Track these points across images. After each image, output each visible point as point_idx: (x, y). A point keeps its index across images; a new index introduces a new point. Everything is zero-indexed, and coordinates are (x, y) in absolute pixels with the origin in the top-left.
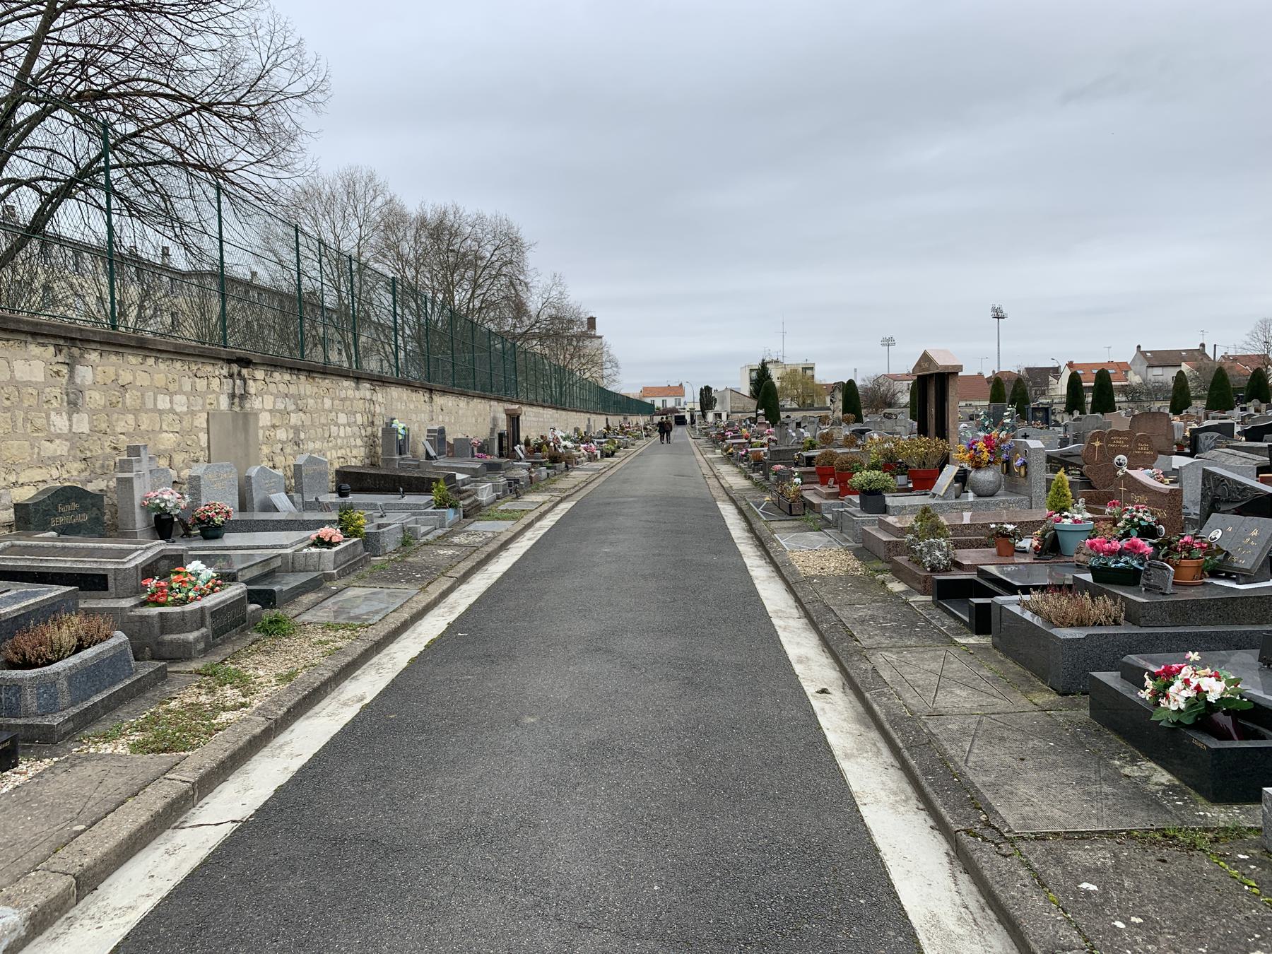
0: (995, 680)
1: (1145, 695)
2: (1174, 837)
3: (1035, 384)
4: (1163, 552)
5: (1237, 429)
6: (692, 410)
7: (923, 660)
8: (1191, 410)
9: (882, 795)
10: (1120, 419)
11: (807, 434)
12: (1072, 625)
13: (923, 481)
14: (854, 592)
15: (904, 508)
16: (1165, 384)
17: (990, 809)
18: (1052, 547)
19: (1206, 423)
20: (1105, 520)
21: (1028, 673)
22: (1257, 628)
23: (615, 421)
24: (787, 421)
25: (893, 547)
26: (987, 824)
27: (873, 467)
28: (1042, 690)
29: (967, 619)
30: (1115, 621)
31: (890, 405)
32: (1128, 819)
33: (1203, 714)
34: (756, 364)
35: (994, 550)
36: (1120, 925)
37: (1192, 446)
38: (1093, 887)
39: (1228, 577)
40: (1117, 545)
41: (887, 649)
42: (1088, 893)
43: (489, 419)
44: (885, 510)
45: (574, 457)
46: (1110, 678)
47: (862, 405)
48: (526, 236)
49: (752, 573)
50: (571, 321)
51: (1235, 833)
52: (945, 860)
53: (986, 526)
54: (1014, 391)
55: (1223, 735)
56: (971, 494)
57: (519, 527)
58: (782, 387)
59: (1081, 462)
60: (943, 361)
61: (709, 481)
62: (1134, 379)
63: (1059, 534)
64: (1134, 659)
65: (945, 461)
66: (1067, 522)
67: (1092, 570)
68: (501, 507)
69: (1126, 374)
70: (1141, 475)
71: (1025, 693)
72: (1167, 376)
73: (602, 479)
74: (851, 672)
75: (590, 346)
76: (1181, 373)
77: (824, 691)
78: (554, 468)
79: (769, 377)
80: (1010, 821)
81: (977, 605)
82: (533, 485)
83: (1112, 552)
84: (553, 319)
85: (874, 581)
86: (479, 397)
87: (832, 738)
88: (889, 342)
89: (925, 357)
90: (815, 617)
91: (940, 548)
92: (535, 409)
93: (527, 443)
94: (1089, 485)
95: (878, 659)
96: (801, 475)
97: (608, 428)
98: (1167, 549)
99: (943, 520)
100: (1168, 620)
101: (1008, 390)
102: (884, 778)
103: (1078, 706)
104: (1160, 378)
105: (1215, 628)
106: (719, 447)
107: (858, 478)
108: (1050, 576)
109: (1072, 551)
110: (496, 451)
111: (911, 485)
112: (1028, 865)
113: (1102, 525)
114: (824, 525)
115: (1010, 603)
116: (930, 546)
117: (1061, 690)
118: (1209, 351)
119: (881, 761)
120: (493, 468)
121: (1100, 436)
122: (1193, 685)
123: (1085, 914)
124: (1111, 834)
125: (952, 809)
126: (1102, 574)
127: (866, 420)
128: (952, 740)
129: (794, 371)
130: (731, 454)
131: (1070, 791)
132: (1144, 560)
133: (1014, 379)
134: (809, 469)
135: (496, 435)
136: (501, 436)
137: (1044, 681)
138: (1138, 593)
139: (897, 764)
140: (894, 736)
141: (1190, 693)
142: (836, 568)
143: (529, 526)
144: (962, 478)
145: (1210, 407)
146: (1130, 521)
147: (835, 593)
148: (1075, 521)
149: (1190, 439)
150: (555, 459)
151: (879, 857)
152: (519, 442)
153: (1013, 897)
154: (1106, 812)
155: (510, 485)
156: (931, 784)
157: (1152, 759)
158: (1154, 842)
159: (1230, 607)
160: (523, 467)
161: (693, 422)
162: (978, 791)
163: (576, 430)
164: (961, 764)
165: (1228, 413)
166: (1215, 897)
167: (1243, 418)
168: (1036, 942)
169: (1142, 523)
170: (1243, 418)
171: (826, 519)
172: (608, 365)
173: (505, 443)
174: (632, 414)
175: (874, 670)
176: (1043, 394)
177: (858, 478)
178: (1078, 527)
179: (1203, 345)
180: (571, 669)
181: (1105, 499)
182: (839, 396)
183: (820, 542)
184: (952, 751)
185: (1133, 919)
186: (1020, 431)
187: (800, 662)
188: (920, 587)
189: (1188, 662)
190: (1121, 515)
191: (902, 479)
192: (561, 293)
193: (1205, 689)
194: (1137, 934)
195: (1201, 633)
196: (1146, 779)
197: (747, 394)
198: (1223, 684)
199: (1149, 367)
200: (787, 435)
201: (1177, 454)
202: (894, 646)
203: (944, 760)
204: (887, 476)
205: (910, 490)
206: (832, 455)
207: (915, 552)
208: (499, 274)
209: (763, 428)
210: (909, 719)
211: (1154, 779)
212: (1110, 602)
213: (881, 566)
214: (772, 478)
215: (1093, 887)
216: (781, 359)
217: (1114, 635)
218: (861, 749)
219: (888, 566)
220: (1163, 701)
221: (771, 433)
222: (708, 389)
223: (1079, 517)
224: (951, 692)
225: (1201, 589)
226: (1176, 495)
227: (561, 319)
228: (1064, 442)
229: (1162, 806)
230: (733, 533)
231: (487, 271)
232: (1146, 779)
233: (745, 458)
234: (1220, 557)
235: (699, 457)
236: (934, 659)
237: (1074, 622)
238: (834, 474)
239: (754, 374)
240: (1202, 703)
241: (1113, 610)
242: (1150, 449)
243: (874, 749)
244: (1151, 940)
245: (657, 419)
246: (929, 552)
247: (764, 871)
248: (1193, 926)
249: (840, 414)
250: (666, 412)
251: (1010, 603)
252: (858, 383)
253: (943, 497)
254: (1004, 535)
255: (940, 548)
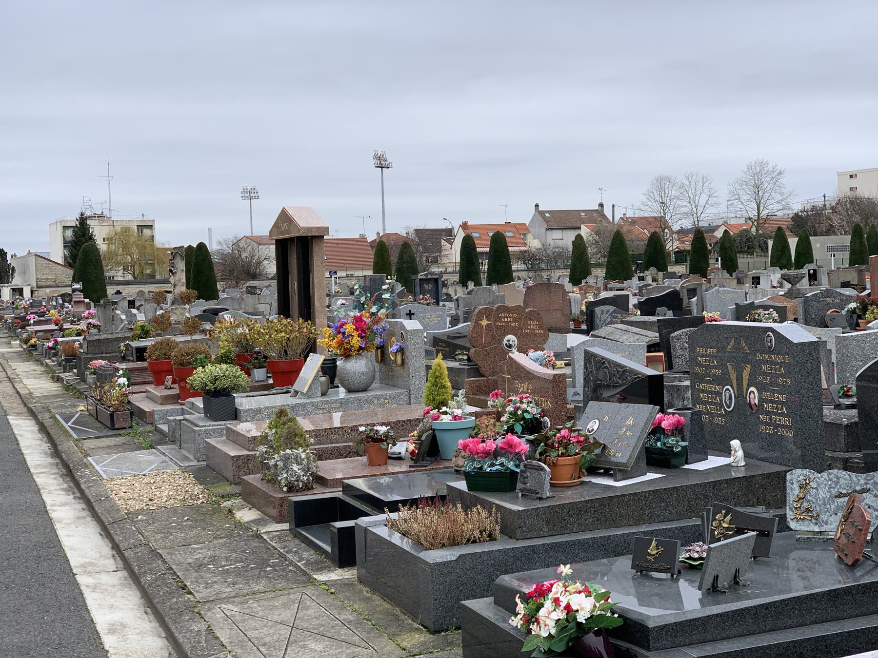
1: (516, 622)
3: (426, 250)
4: (539, 450)
5: (633, 301)
7: (273, 608)
8: (590, 280)
10: (513, 293)
12: (444, 546)
13: (284, 375)
14: (192, 527)
15: (257, 408)
16: (564, 249)
18: (430, 450)
19: (604, 295)
20: (489, 414)
21: (397, 611)
24: (116, 298)
25: (244, 464)
27: (224, 359)
28: (412, 630)
29: (328, 548)
30: (490, 536)
31: (254, 276)
34: (72, 220)
35: (365, 459)
37: (588, 323)
39: (607, 473)
41: (228, 600)
44: (235, 415)
46: (481, 606)
47: (219, 275)
49: (53, 515)
53: (355, 429)
54: (401, 257)
56: (342, 390)
58: (109, 252)
59: (468, 345)
60: (305, 222)
62: (534, 244)
63: (437, 434)
64: (508, 580)
65: (312, 348)
66: (446, 419)
69: (525, 239)
70: (528, 361)
71: (392, 637)
72: (565, 240)
74: (180, 637)
76: (579, 237)
79: (91, 238)
81: (340, 529)
83: (487, 454)
85: (218, 510)
88: (250, 195)
89: (284, 217)
94: (476, 371)
96: (128, 374)
99: (305, 424)
100: (545, 529)
101: (394, 258)
103: (451, 644)
104: (560, 243)
106: (17, 337)
107: (200, 376)
108: (429, 486)
109: (451, 454)
111: (271, 381)
114: (159, 439)
115: (375, 524)
116: (286, 459)
117: (432, 626)
118: (608, 212)
121: (487, 313)
122: (563, 604)
127: (222, 295)
129: (126, 231)
130: (34, 346)
132: (520, 460)
133: (401, 243)
134: (140, 364)
137: (414, 616)
138: (514, 501)
141: (561, 614)
142: (169, 498)
144: (329, 369)
145: (609, 276)
146: (514, 414)
147: (166, 531)
148: (455, 418)
149: (587, 314)
165: (626, 283)
167: (641, 289)
169: (527, 416)
170: (641, 289)
171: (161, 432)
175: (210, 630)
176: (435, 261)
177: (200, 376)
178: (459, 424)
179: (601, 205)
181: (488, 389)
182: (181, 265)
183: (150, 463)
186: (403, 308)
187: (112, 631)
188: (274, 512)
189: (559, 577)
190: (504, 407)
191: (259, 374)
193: (574, 608)
195: (557, 544)
198: (591, 600)
199: (548, 229)
200: (113, 319)
204: (236, 370)
205: (268, 387)
206: (170, 345)
207: (269, 468)
209: (81, 308)
212: (484, 513)
213: (229, 489)
214: (90, 378)
216: (106, 213)
217: (489, 553)
220: (534, 627)
221: (92, 314)
223: (458, 412)
224: (304, 647)
225: (580, 490)
226: (559, 381)
228: (455, 321)
233: (52, 352)
234: (598, 451)
236: (286, 606)
237: (445, 541)
238: (167, 368)
239: (69, 234)
241: (487, 524)
242: (541, 328)
246: (286, 468)
249: (184, 289)
251: (376, 524)
252: (213, 247)
253: (307, 395)
254: (375, 440)
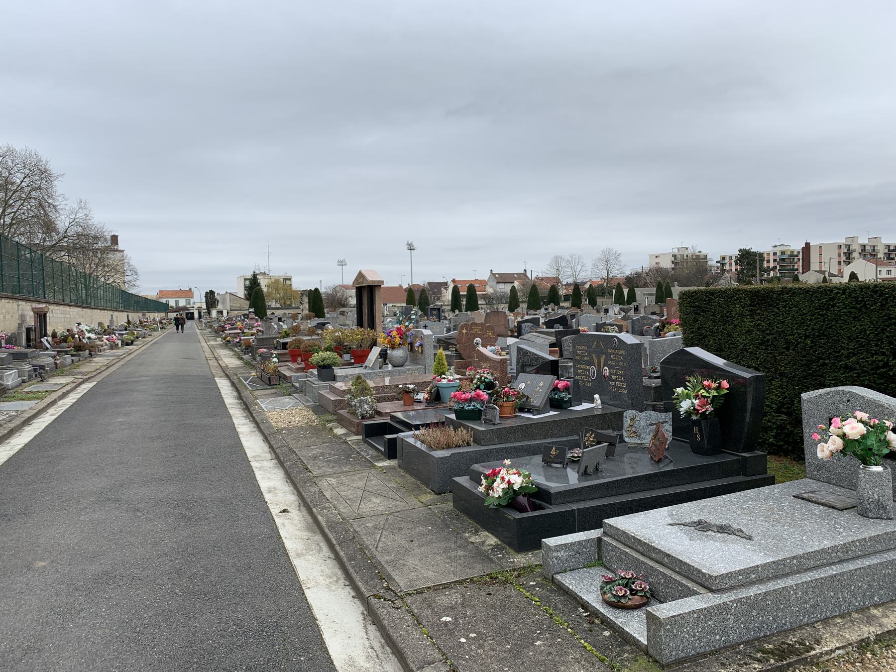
0: (398, 489)
1: (482, 489)
2: (497, 578)
5: (542, 321)
6: (199, 309)
8: (519, 310)
9: (321, 580)
11: (285, 327)
13: (360, 358)
14: (311, 437)
15: (346, 375)
17: (390, 578)
18: (436, 398)
19: (526, 317)
21: (419, 482)
22: (543, 441)
23: (135, 317)
25: (339, 404)
26: (388, 589)
27: (327, 349)
29: (383, 449)
31: (344, 306)
32: (471, 571)
33: (512, 498)
34: (249, 275)
35: (402, 402)
36: (463, 640)
37: (518, 332)
38: (449, 619)
39: (529, 411)
40: (468, 395)
41: (330, 476)
42: (446, 623)
43: (16, 316)
44: (334, 378)
45: (98, 346)
47: (325, 305)
48: (54, 167)
49: (238, 430)
50: (96, 238)
51: (529, 569)
52: (361, 617)
53: (397, 386)
55: (522, 510)
56: (390, 365)
57: (42, 405)
58: (268, 292)
60: (371, 278)
61: (210, 362)
62: (490, 290)
64: (477, 467)
65: (374, 343)
66: (444, 381)
67: (456, 412)
68: (27, 390)
70: (487, 351)
71: (416, 496)
72: (506, 288)
73: (121, 363)
75: (113, 258)
76: (513, 287)
77: (285, 511)
78: (79, 355)
79: (259, 285)
80: (402, 584)
82: (58, 370)
83: (466, 400)
84: (79, 235)
85: (325, 428)
86: (7, 298)
87: (288, 544)
88: (342, 263)
89: (360, 275)
90: (284, 458)
91: (367, 403)
92: (62, 308)
93: (54, 335)
94: (460, 357)
95: (323, 483)
97: (129, 322)
98: (496, 396)
99: (371, 384)
101: (417, 297)
102: (323, 567)
105: (517, 443)
107: (316, 357)
109: (447, 400)
110: (24, 342)
112: (411, 612)
113: (465, 382)
115: (408, 436)
116: (361, 402)
119: (322, 555)
120: (19, 357)
123: (443, 637)
124: (461, 582)
125: (366, 582)
126: (462, 415)
127: (327, 316)
128: (369, 534)
129: (277, 281)
131: (439, 558)
135: (24, 329)
136: (28, 330)
137: (427, 486)
139: (332, 556)
140: (331, 536)
141: (505, 486)
142: (299, 421)
143: (53, 403)
144: (383, 355)
145: (529, 308)
146: (480, 379)
148: (449, 381)
150: (79, 348)
151: (315, 624)
152: (46, 335)
153: (401, 635)
154: (459, 568)
155: (35, 370)
156: (353, 567)
157: (487, 529)
158: (486, 583)
159: (529, 430)
160: (49, 356)
161: (200, 317)
162: (383, 567)
163: (100, 324)
164: (373, 549)
165: (538, 312)
166: (516, 611)
168: (413, 662)
171: (293, 386)
172: (129, 273)
173: (32, 336)
174: (150, 311)
175: (320, 491)
176: (438, 299)
177: (316, 357)
178: (451, 384)
180: (82, 518)
181: (466, 366)
182: (306, 300)
183: (290, 403)
184: (368, 541)
185: (471, 635)
187: (269, 491)
188: (354, 430)
189: (504, 466)
190: (475, 375)
191: (347, 357)
192: (86, 216)
194: (472, 644)
196: (483, 543)
197: (243, 297)
199: (498, 283)
201: (511, 336)
202: (335, 473)
203: (363, 549)
204: (335, 355)
205: (351, 364)
206: (300, 341)
208: (28, 197)
209: (253, 322)
210: (341, 523)
211: (487, 543)
212: (465, 432)
213: (330, 417)
214: (258, 358)
215: (449, 619)
216: (267, 272)
218: (308, 549)
219: (335, 417)
220: (491, 492)
221: (259, 325)
222: (212, 292)
223: (451, 378)
224: (370, 501)
226: (503, 362)
227: (87, 236)
228: (448, 330)
229: (490, 559)
230: (225, 400)
231: (17, 194)
232: (483, 543)
233: (238, 344)
234: (524, 399)
235: (204, 344)
236: (360, 479)
238: (298, 354)
239: (248, 282)
240: (511, 491)
243: (318, 548)
244: (481, 646)
245: (173, 315)
246: (361, 407)
247: (231, 650)
248: (503, 632)
250: (178, 310)
251: (408, 437)
252: (322, 290)
253: (372, 368)
254: (408, 392)
255: (367, 403)
